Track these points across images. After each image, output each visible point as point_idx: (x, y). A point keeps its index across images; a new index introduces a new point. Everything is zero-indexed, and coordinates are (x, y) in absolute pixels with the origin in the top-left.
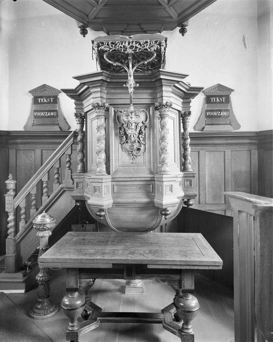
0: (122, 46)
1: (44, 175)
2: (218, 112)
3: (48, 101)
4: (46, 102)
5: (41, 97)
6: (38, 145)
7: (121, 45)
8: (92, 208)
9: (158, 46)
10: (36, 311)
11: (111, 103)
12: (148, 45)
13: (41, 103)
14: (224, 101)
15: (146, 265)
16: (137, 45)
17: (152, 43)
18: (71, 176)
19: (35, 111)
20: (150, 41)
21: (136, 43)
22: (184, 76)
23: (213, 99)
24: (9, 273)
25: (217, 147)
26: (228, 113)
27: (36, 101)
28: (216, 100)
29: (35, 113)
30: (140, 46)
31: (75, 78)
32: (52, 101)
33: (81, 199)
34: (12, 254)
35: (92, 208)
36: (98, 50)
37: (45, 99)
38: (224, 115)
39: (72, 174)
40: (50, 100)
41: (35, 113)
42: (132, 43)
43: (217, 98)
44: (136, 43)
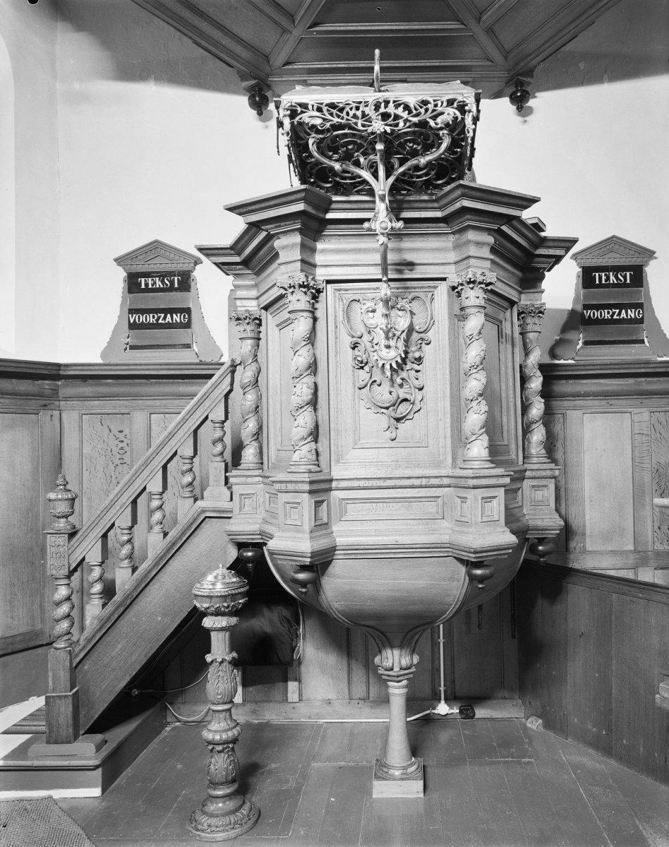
0: (359, 113)
1: (151, 476)
2: (614, 310)
3: (167, 285)
4: (162, 286)
5: (147, 275)
6: (140, 401)
7: (354, 111)
8: (280, 562)
9: (458, 114)
10: (204, 820)
11: (328, 278)
12: (430, 111)
13: (147, 290)
14: (628, 281)
15: (298, 679)
16: (400, 111)
17: (440, 104)
18: (227, 479)
19: (131, 311)
20: (434, 101)
21: (397, 106)
22: (529, 201)
23: (599, 275)
24: (56, 742)
25: (612, 402)
26: (639, 311)
27: (133, 283)
28: (608, 278)
29: (130, 316)
30: (407, 112)
31: (231, 209)
32: (176, 286)
33: (252, 539)
34: (66, 692)
35: (280, 562)
36: (292, 124)
37: (157, 279)
38: (629, 317)
39: (227, 474)
40: (172, 282)
41: (130, 316)
42: (386, 107)
43: (611, 274)
44: (397, 106)
